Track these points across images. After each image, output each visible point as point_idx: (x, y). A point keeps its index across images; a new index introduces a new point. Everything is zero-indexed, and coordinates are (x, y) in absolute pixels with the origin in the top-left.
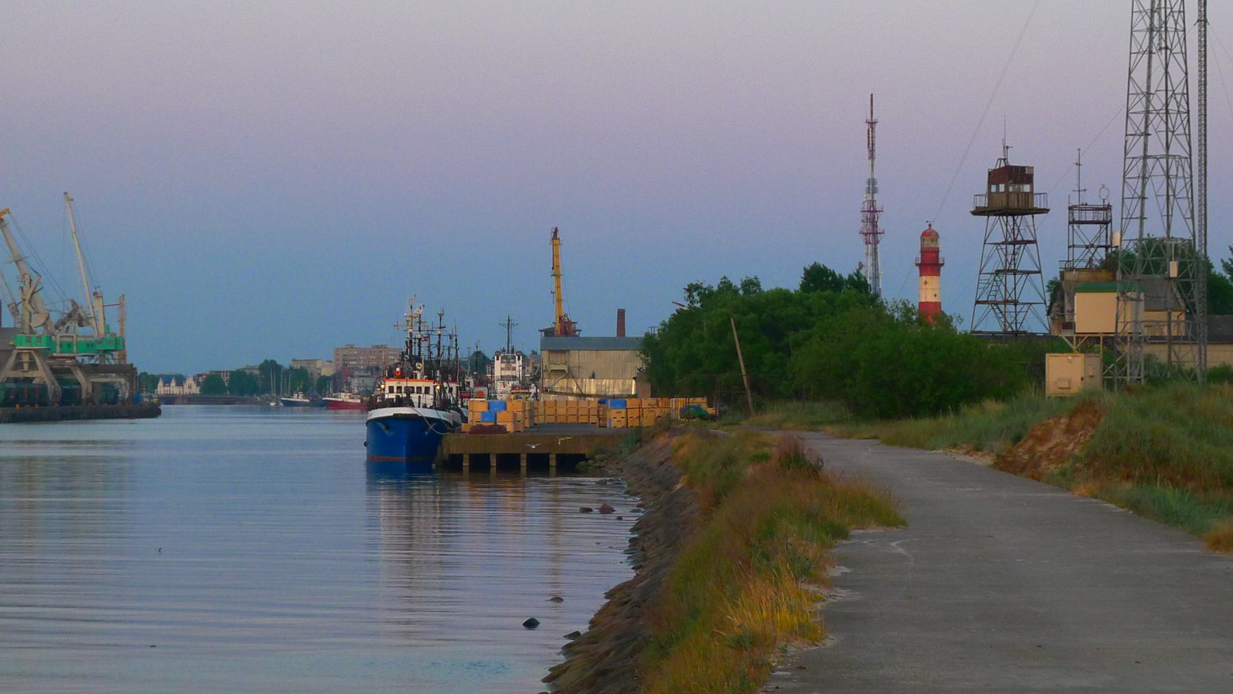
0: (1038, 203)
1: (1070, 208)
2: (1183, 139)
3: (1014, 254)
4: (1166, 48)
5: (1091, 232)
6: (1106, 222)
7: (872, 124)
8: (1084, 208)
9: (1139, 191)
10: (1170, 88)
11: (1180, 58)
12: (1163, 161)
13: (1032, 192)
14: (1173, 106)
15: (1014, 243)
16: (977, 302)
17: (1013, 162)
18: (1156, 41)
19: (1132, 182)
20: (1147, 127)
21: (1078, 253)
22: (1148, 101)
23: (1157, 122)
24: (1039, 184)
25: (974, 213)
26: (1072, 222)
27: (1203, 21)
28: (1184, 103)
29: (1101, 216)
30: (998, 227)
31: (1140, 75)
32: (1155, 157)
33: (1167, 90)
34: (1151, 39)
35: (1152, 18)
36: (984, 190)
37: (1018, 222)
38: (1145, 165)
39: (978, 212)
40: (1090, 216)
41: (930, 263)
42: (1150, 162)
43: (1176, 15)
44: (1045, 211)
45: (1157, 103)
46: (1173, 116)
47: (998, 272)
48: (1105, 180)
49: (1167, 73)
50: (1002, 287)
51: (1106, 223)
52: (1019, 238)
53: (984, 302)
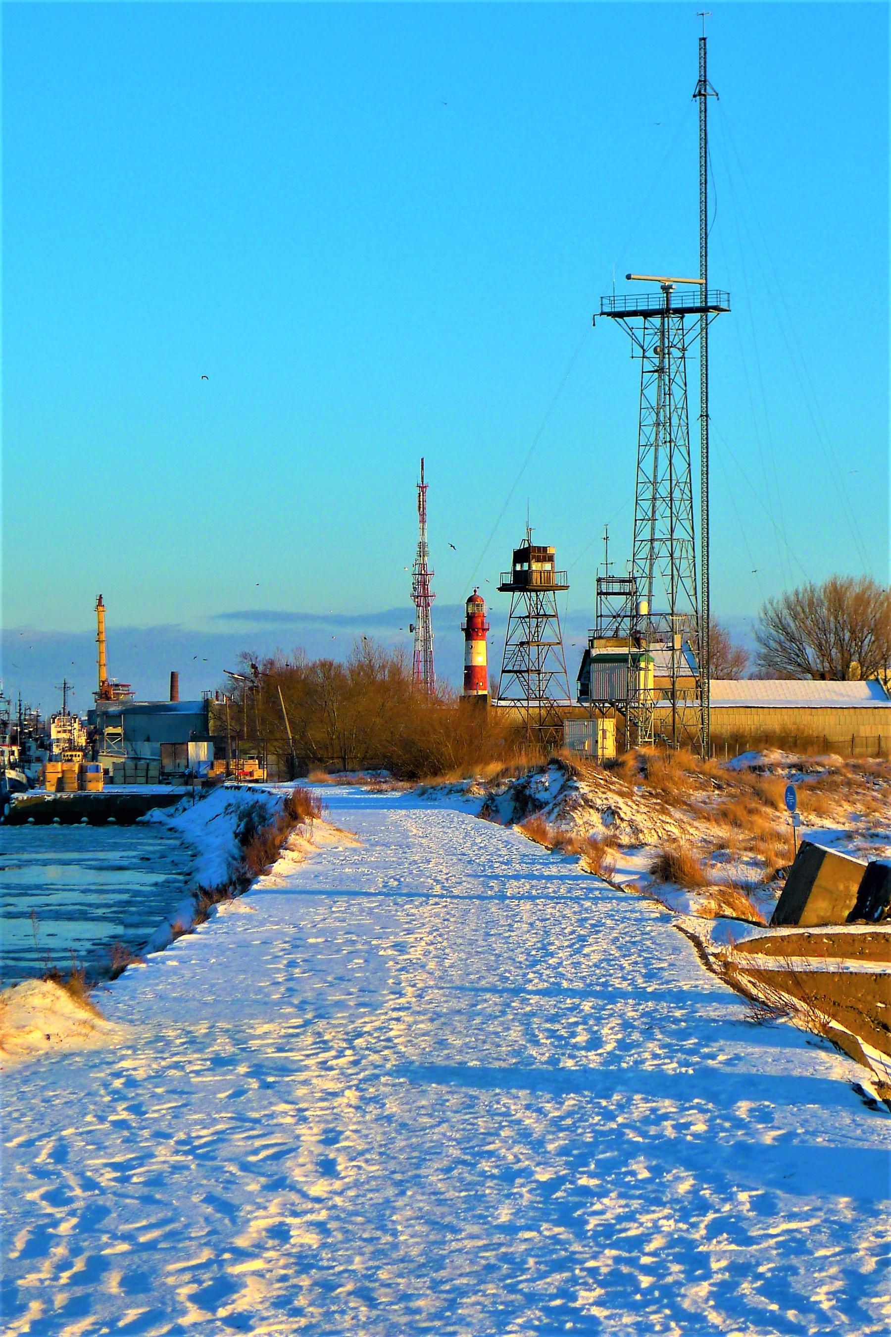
0: (558, 580)
1: (599, 580)
2: (687, 525)
3: (537, 626)
7: (423, 488)
8: (611, 580)
9: (647, 570)
10: (674, 477)
11: (684, 450)
14: (677, 494)
15: (538, 616)
16: (504, 671)
18: (661, 435)
19: (641, 563)
20: (654, 512)
22: (656, 490)
23: (662, 507)
24: (559, 565)
25: (501, 589)
26: (600, 593)
27: (705, 416)
28: (687, 491)
29: (627, 587)
30: (521, 602)
31: (648, 465)
32: (661, 540)
33: (671, 480)
35: (658, 414)
36: (510, 569)
37: (541, 597)
38: (652, 548)
39: (504, 588)
40: (616, 587)
41: (473, 629)
42: (656, 544)
43: (679, 411)
44: (566, 588)
45: (663, 491)
46: (677, 503)
47: (522, 644)
49: (670, 464)
52: (542, 612)
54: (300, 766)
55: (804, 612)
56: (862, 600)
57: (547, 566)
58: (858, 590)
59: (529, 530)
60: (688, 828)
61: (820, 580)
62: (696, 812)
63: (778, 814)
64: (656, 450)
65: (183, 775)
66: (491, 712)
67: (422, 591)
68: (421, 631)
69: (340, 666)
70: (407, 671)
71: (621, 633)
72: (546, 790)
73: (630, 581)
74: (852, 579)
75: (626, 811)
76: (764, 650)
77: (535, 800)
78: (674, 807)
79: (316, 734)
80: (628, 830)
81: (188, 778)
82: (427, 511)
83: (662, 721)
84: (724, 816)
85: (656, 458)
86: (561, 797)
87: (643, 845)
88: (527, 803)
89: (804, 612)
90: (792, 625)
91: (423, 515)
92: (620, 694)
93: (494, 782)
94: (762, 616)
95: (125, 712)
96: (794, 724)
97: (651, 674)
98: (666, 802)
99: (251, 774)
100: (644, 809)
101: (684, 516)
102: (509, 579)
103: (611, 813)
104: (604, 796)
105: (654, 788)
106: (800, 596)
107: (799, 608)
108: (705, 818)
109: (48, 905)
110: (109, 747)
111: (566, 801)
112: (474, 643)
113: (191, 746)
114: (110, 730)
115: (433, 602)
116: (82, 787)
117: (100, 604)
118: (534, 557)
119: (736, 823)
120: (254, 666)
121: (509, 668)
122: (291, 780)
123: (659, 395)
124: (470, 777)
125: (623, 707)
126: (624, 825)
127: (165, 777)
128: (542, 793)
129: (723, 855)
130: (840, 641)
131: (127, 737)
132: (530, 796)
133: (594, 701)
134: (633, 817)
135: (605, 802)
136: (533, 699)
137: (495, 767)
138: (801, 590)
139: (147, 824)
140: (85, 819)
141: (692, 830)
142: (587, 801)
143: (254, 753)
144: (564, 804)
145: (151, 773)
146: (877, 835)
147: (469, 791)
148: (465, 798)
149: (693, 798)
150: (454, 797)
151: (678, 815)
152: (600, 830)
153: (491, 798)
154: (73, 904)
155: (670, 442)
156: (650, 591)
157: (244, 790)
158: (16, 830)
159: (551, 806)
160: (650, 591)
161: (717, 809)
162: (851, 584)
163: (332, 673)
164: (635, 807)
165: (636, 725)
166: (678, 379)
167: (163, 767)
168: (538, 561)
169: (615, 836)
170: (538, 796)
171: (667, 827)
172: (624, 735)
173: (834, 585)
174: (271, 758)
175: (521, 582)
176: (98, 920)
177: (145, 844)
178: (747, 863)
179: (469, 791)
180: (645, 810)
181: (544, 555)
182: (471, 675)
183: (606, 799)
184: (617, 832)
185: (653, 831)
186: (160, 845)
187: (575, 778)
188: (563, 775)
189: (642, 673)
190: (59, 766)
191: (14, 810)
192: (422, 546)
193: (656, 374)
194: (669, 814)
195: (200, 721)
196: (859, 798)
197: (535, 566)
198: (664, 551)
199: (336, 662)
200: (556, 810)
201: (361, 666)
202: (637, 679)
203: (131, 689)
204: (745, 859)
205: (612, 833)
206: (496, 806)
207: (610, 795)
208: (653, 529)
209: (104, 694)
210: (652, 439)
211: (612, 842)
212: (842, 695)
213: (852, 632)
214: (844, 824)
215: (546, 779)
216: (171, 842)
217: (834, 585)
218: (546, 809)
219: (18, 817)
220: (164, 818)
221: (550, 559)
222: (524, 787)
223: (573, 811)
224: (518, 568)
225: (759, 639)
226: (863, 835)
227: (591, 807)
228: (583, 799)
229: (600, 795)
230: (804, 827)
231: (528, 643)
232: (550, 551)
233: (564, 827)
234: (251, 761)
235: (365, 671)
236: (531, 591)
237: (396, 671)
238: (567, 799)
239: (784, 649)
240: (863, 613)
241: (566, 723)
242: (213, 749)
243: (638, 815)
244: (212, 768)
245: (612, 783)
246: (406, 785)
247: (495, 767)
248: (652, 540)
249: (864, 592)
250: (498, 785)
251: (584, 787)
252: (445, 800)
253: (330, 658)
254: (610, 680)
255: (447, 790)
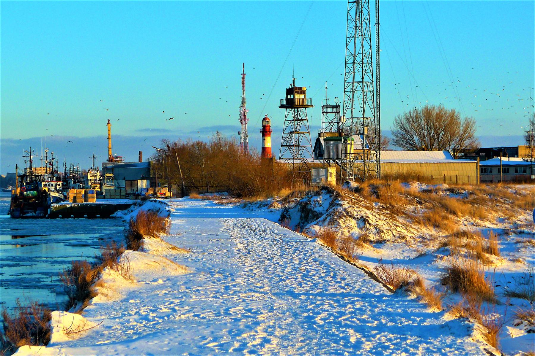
0: (308, 103)
1: (323, 107)
4: (362, 35)
5: (331, 116)
6: (338, 113)
7: (243, 75)
8: (328, 106)
9: (351, 97)
10: (364, 52)
11: (368, 39)
12: (361, 84)
13: (305, 98)
14: (365, 60)
15: (298, 120)
16: (282, 146)
17: (296, 86)
18: (358, 32)
19: (348, 93)
20: (354, 69)
21: (326, 125)
25: (280, 107)
26: (323, 113)
28: (370, 59)
29: (335, 110)
30: (290, 113)
31: (351, 47)
34: (356, 31)
35: (356, 22)
36: (285, 97)
37: (299, 111)
38: (353, 86)
39: (282, 107)
40: (331, 110)
41: (265, 131)
42: (355, 84)
45: (359, 59)
47: (291, 133)
48: (336, 95)
50: (293, 139)
51: (338, 113)
52: (300, 118)
53: (285, 146)
54: (187, 190)
55: (413, 121)
56: (439, 116)
57: (302, 96)
58: (437, 111)
59: (294, 79)
60: (410, 229)
61: (420, 107)
62: (412, 218)
63: (459, 219)
64: (355, 39)
65: (134, 195)
66: (275, 166)
67: (243, 119)
68: (243, 135)
69: (206, 144)
70: (237, 145)
71: (333, 130)
72: (321, 205)
73: (336, 107)
74: (434, 107)
75: (372, 219)
76: (395, 138)
77: (313, 212)
78: (398, 215)
79: (195, 176)
80: (374, 231)
81: (137, 196)
82: (245, 85)
83: (359, 169)
84: (428, 221)
85: (355, 43)
86: (331, 210)
87: (385, 241)
88: (308, 214)
89: (413, 121)
90: (408, 127)
91: (244, 87)
92: (338, 156)
93: (286, 200)
94: (395, 122)
95: (113, 167)
96: (413, 170)
97: (353, 146)
98: (393, 213)
99: (164, 194)
100: (383, 218)
101: (369, 71)
102: (284, 103)
103: (363, 221)
104: (358, 210)
105: (385, 204)
106: (412, 114)
107: (411, 120)
108: (418, 222)
109: (23, 274)
110: (107, 182)
111: (334, 213)
112: (266, 138)
113: (139, 181)
114: (108, 175)
115: (249, 124)
116: (86, 201)
117: (109, 123)
118: (296, 92)
119: (436, 226)
120: (168, 146)
121: (285, 144)
122: (182, 197)
123: (356, 13)
124: (271, 197)
125: (339, 161)
126: (371, 227)
127: (127, 196)
128: (318, 207)
129: (447, 250)
130: (429, 134)
131: (115, 178)
132: (310, 209)
133: (325, 159)
134: (377, 223)
135: (359, 213)
136: (297, 159)
137: (285, 192)
138: (412, 111)
139: (113, 217)
140: (86, 216)
141: (413, 231)
142: (347, 213)
143: (167, 185)
144: (333, 215)
145: (122, 194)
146: (523, 232)
147: (272, 206)
148: (269, 210)
149: (407, 210)
150: (263, 209)
151: (401, 220)
152: (356, 231)
153: (286, 210)
154: (39, 273)
155: (362, 35)
156: (352, 107)
157: (158, 202)
158: (54, 221)
159: (325, 215)
160: (352, 107)
161: (422, 217)
162: (433, 109)
163: (202, 147)
164: (378, 216)
165: (345, 170)
166: (365, 6)
167: (126, 191)
168: (298, 94)
169: (366, 235)
170: (315, 209)
171: (398, 229)
172: (340, 176)
173: (427, 109)
174: (174, 187)
175: (290, 104)
176: (43, 288)
177: (105, 229)
178: (466, 257)
179: (272, 206)
180: (384, 218)
181: (301, 91)
182: (264, 149)
183: (360, 211)
184: (367, 232)
185: (389, 232)
186: (114, 230)
187: (339, 199)
188: (331, 196)
189: (349, 146)
190: (75, 191)
191: (52, 212)
192: (243, 99)
193: (355, 4)
194: (395, 220)
195: (147, 171)
196: (498, 208)
197: (297, 96)
198: (359, 88)
199: (204, 142)
200: (328, 219)
201: (215, 144)
202: (346, 149)
203: (123, 158)
204: (462, 253)
205: (363, 233)
206: (289, 215)
207: (361, 209)
208: (354, 77)
209: (110, 160)
210: (353, 34)
211: (366, 240)
212: (432, 158)
213: (435, 130)
214: (497, 225)
215: (320, 199)
216: (121, 228)
217: (427, 109)
218: (321, 219)
219: (54, 215)
220: (122, 215)
221: (304, 93)
222: (307, 204)
223: (339, 219)
224: (289, 97)
225: (393, 133)
226: (514, 232)
227: (350, 216)
228: (345, 211)
229: (356, 209)
230: (474, 227)
231: (294, 132)
232: (304, 89)
233: (334, 229)
234: (164, 188)
235: (217, 146)
236: (295, 108)
237: (232, 146)
238: (335, 211)
239: (405, 138)
240: (439, 122)
241: (313, 170)
242: (149, 183)
243: (380, 221)
244: (147, 191)
245: (361, 201)
246: (236, 200)
247: (285, 192)
248: (353, 82)
249: (440, 112)
250: (289, 202)
251: (346, 204)
252: (258, 212)
253: (200, 140)
254: (333, 149)
255: (258, 205)
